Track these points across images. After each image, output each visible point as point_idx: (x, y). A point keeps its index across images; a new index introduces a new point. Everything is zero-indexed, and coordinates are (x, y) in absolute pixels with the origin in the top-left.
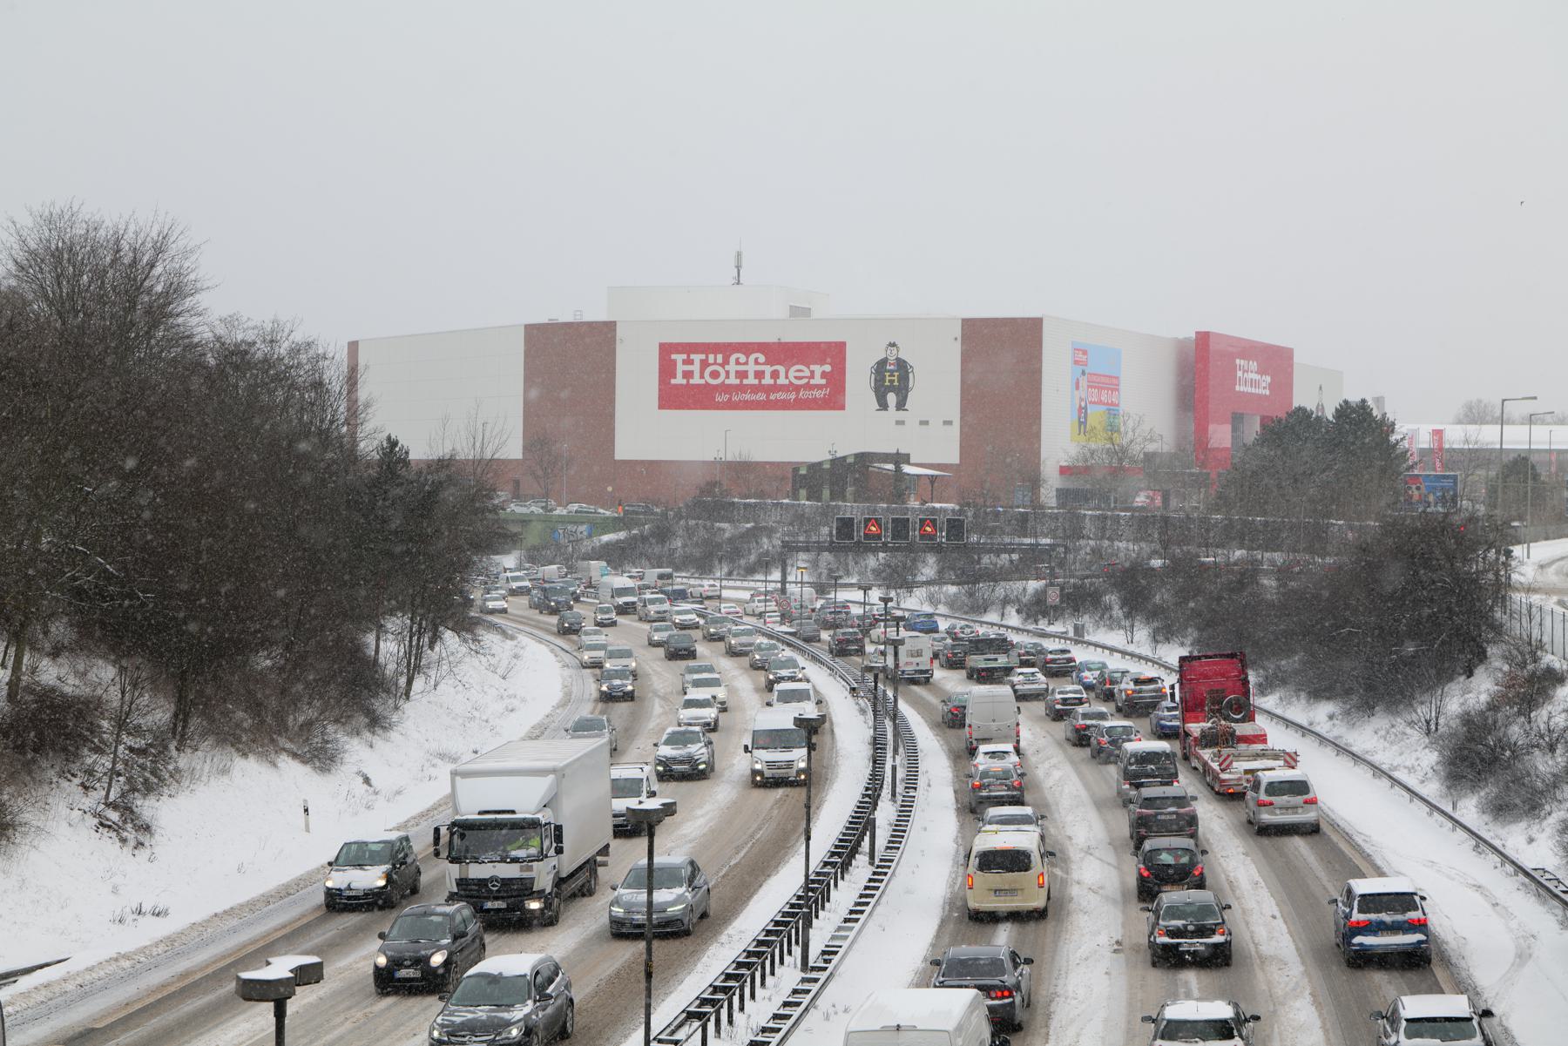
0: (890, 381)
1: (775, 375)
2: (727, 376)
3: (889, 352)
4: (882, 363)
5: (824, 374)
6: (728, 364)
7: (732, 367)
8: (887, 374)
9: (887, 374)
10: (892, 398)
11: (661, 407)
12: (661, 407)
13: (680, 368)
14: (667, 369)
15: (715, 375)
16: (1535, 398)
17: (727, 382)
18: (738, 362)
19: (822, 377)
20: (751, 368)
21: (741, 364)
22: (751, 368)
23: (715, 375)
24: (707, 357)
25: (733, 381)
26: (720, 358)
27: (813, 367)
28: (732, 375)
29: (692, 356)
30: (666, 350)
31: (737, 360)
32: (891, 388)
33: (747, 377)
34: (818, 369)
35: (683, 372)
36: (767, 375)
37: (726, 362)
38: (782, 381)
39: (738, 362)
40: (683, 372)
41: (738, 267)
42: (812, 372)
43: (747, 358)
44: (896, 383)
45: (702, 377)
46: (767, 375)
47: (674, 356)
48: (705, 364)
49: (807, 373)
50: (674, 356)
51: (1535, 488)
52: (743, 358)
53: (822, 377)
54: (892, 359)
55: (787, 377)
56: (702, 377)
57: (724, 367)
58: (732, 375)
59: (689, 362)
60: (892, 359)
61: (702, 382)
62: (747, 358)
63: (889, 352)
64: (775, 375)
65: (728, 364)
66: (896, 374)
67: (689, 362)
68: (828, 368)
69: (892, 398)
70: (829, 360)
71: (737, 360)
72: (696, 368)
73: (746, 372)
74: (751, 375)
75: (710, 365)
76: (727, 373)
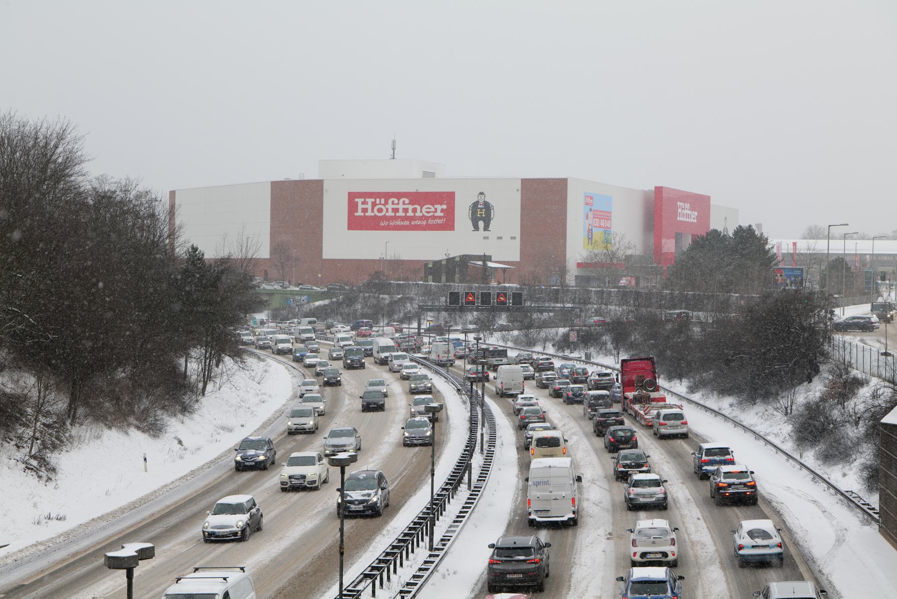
0: (480, 214)
1: (414, 210)
2: (387, 211)
3: (479, 198)
4: (476, 204)
5: (442, 210)
7: (390, 206)
8: (479, 210)
9: (484, 216)
10: (481, 224)
13: (360, 206)
14: (352, 207)
15: (380, 210)
16: (847, 225)
17: (387, 214)
18: (393, 203)
20: (401, 207)
22: (401, 207)
23: (380, 210)
24: (375, 200)
27: (436, 206)
28: (390, 210)
30: (352, 196)
31: (393, 202)
32: (481, 218)
33: (398, 212)
34: (439, 207)
35: (362, 208)
36: (410, 211)
37: (386, 203)
39: (393, 203)
40: (362, 208)
42: (436, 209)
44: (484, 216)
45: (373, 211)
47: (356, 200)
49: (433, 210)
50: (356, 200)
52: (396, 201)
54: (481, 201)
55: (421, 212)
56: (373, 211)
58: (390, 210)
60: (481, 201)
61: (373, 214)
63: (479, 198)
66: (484, 210)
67: (365, 210)
68: (444, 207)
69: (481, 224)
70: (445, 202)
71: (393, 202)
72: (369, 206)
73: (403, 209)
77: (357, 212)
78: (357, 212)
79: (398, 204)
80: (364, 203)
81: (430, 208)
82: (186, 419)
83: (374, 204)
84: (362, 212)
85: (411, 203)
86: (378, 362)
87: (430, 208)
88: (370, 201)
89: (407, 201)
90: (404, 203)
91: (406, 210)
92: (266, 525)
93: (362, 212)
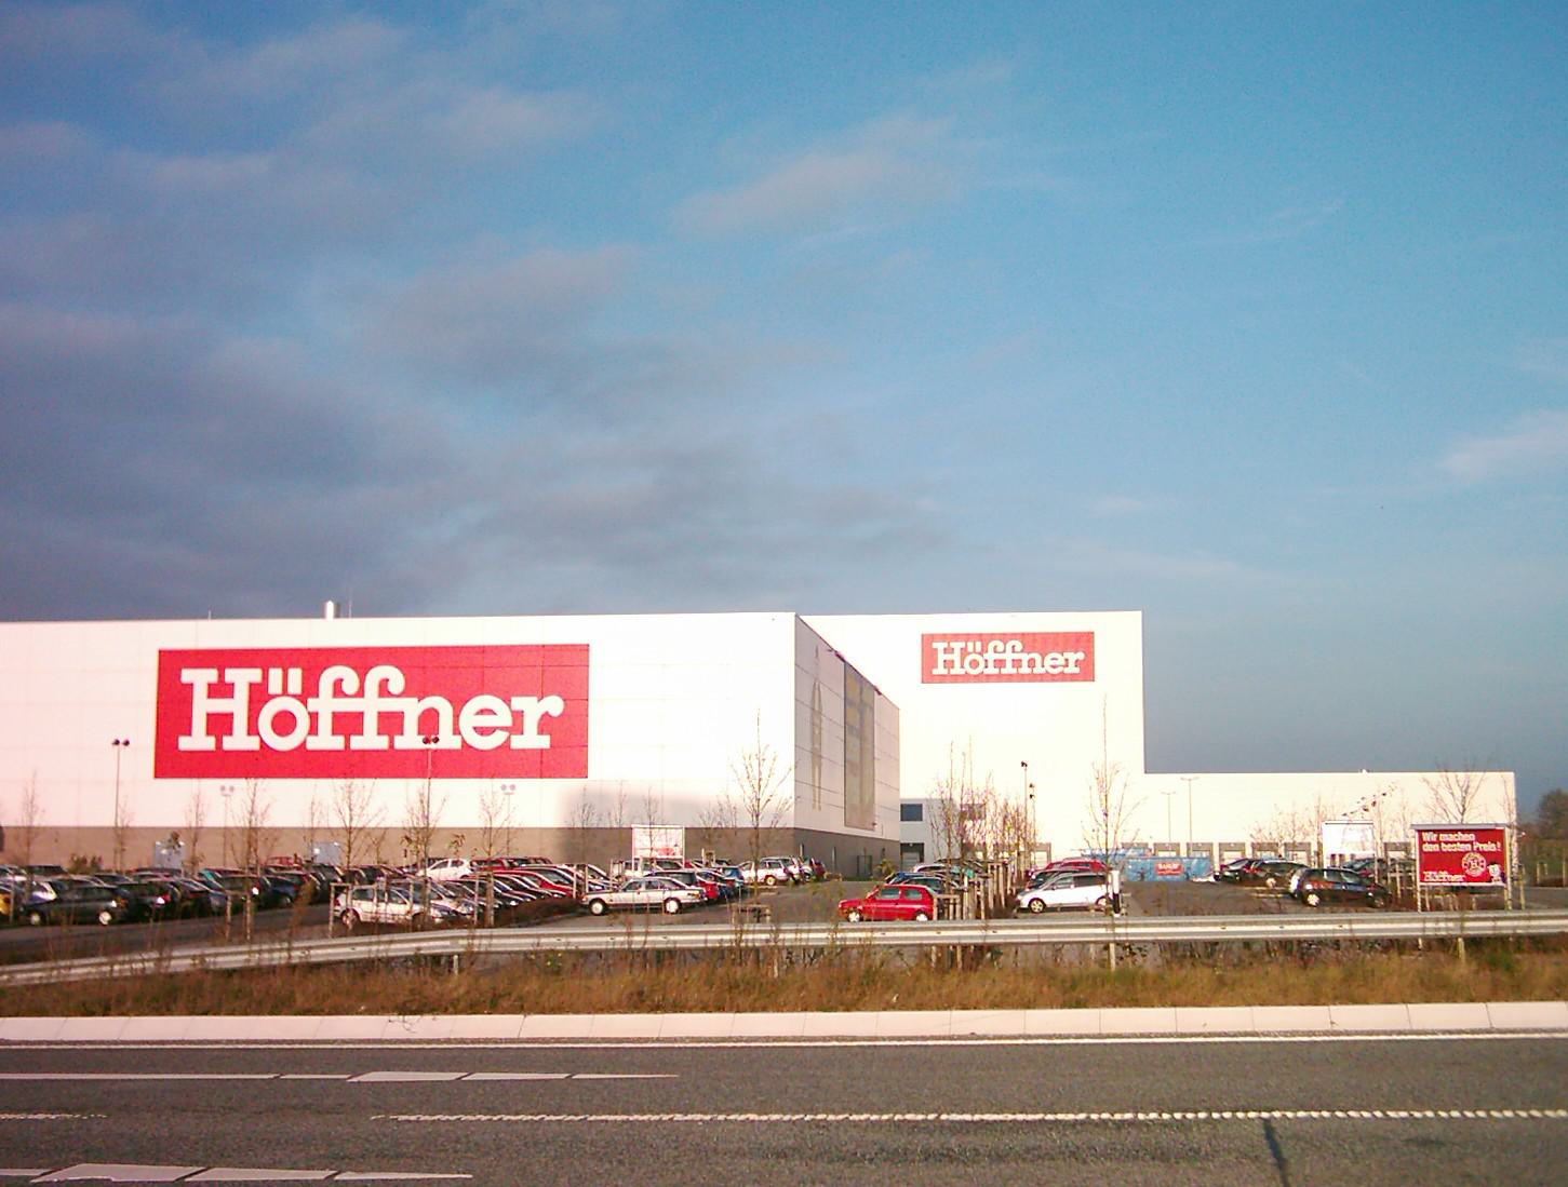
1: (1032, 663)
2: (313, 730)
6: (316, 695)
7: (991, 656)
11: (156, 776)
12: (156, 776)
13: (941, 657)
14: (173, 708)
15: (284, 723)
17: (314, 744)
18: (338, 691)
19: (541, 731)
21: (390, 695)
22: (371, 706)
24: (265, 677)
25: (326, 740)
26: (978, 644)
27: (518, 703)
28: (991, 664)
29: (953, 645)
31: (338, 684)
35: (209, 716)
36: (1025, 664)
38: (447, 741)
40: (209, 716)
41: (1104, 715)
42: (518, 716)
43: (1005, 644)
45: (253, 729)
46: (1025, 664)
48: (964, 652)
49: (504, 719)
50: (935, 645)
51: (1526, 907)
53: (541, 731)
55: (457, 731)
56: (253, 729)
57: (305, 703)
58: (991, 664)
59: (221, 690)
61: (253, 744)
62: (1005, 644)
64: (1032, 663)
65: (316, 695)
68: (1080, 656)
71: (338, 684)
73: (229, 717)
74: (1009, 664)
75: (969, 653)
76: (314, 717)
77: (189, 733)
78: (189, 733)
79: (360, 693)
80: (221, 690)
81: (491, 712)
82: (723, 799)
83: (259, 695)
84: (335, 732)
85: (414, 689)
86: (263, 904)
87: (491, 712)
88: (242, 678)
89: (1019, 646)
90: (384, 691)
91: (391, 723)
92: (704, 823)
93: (335, 732)
